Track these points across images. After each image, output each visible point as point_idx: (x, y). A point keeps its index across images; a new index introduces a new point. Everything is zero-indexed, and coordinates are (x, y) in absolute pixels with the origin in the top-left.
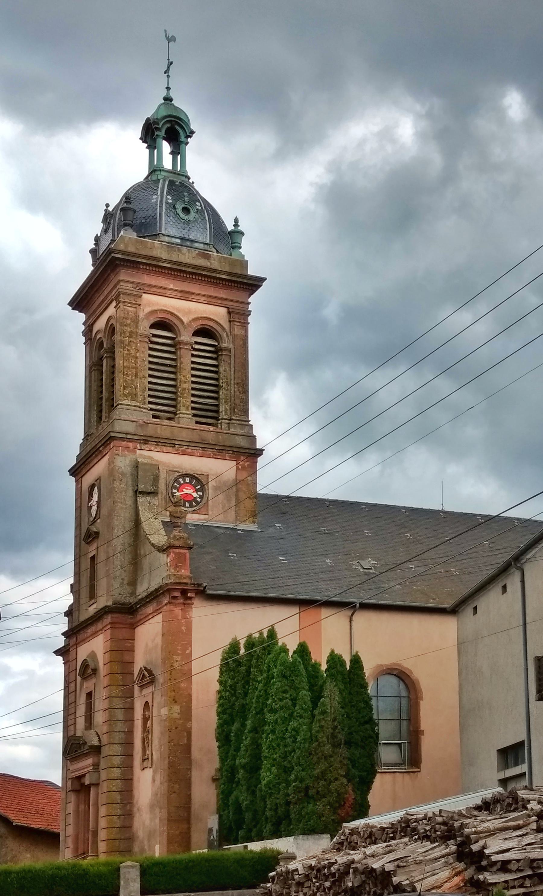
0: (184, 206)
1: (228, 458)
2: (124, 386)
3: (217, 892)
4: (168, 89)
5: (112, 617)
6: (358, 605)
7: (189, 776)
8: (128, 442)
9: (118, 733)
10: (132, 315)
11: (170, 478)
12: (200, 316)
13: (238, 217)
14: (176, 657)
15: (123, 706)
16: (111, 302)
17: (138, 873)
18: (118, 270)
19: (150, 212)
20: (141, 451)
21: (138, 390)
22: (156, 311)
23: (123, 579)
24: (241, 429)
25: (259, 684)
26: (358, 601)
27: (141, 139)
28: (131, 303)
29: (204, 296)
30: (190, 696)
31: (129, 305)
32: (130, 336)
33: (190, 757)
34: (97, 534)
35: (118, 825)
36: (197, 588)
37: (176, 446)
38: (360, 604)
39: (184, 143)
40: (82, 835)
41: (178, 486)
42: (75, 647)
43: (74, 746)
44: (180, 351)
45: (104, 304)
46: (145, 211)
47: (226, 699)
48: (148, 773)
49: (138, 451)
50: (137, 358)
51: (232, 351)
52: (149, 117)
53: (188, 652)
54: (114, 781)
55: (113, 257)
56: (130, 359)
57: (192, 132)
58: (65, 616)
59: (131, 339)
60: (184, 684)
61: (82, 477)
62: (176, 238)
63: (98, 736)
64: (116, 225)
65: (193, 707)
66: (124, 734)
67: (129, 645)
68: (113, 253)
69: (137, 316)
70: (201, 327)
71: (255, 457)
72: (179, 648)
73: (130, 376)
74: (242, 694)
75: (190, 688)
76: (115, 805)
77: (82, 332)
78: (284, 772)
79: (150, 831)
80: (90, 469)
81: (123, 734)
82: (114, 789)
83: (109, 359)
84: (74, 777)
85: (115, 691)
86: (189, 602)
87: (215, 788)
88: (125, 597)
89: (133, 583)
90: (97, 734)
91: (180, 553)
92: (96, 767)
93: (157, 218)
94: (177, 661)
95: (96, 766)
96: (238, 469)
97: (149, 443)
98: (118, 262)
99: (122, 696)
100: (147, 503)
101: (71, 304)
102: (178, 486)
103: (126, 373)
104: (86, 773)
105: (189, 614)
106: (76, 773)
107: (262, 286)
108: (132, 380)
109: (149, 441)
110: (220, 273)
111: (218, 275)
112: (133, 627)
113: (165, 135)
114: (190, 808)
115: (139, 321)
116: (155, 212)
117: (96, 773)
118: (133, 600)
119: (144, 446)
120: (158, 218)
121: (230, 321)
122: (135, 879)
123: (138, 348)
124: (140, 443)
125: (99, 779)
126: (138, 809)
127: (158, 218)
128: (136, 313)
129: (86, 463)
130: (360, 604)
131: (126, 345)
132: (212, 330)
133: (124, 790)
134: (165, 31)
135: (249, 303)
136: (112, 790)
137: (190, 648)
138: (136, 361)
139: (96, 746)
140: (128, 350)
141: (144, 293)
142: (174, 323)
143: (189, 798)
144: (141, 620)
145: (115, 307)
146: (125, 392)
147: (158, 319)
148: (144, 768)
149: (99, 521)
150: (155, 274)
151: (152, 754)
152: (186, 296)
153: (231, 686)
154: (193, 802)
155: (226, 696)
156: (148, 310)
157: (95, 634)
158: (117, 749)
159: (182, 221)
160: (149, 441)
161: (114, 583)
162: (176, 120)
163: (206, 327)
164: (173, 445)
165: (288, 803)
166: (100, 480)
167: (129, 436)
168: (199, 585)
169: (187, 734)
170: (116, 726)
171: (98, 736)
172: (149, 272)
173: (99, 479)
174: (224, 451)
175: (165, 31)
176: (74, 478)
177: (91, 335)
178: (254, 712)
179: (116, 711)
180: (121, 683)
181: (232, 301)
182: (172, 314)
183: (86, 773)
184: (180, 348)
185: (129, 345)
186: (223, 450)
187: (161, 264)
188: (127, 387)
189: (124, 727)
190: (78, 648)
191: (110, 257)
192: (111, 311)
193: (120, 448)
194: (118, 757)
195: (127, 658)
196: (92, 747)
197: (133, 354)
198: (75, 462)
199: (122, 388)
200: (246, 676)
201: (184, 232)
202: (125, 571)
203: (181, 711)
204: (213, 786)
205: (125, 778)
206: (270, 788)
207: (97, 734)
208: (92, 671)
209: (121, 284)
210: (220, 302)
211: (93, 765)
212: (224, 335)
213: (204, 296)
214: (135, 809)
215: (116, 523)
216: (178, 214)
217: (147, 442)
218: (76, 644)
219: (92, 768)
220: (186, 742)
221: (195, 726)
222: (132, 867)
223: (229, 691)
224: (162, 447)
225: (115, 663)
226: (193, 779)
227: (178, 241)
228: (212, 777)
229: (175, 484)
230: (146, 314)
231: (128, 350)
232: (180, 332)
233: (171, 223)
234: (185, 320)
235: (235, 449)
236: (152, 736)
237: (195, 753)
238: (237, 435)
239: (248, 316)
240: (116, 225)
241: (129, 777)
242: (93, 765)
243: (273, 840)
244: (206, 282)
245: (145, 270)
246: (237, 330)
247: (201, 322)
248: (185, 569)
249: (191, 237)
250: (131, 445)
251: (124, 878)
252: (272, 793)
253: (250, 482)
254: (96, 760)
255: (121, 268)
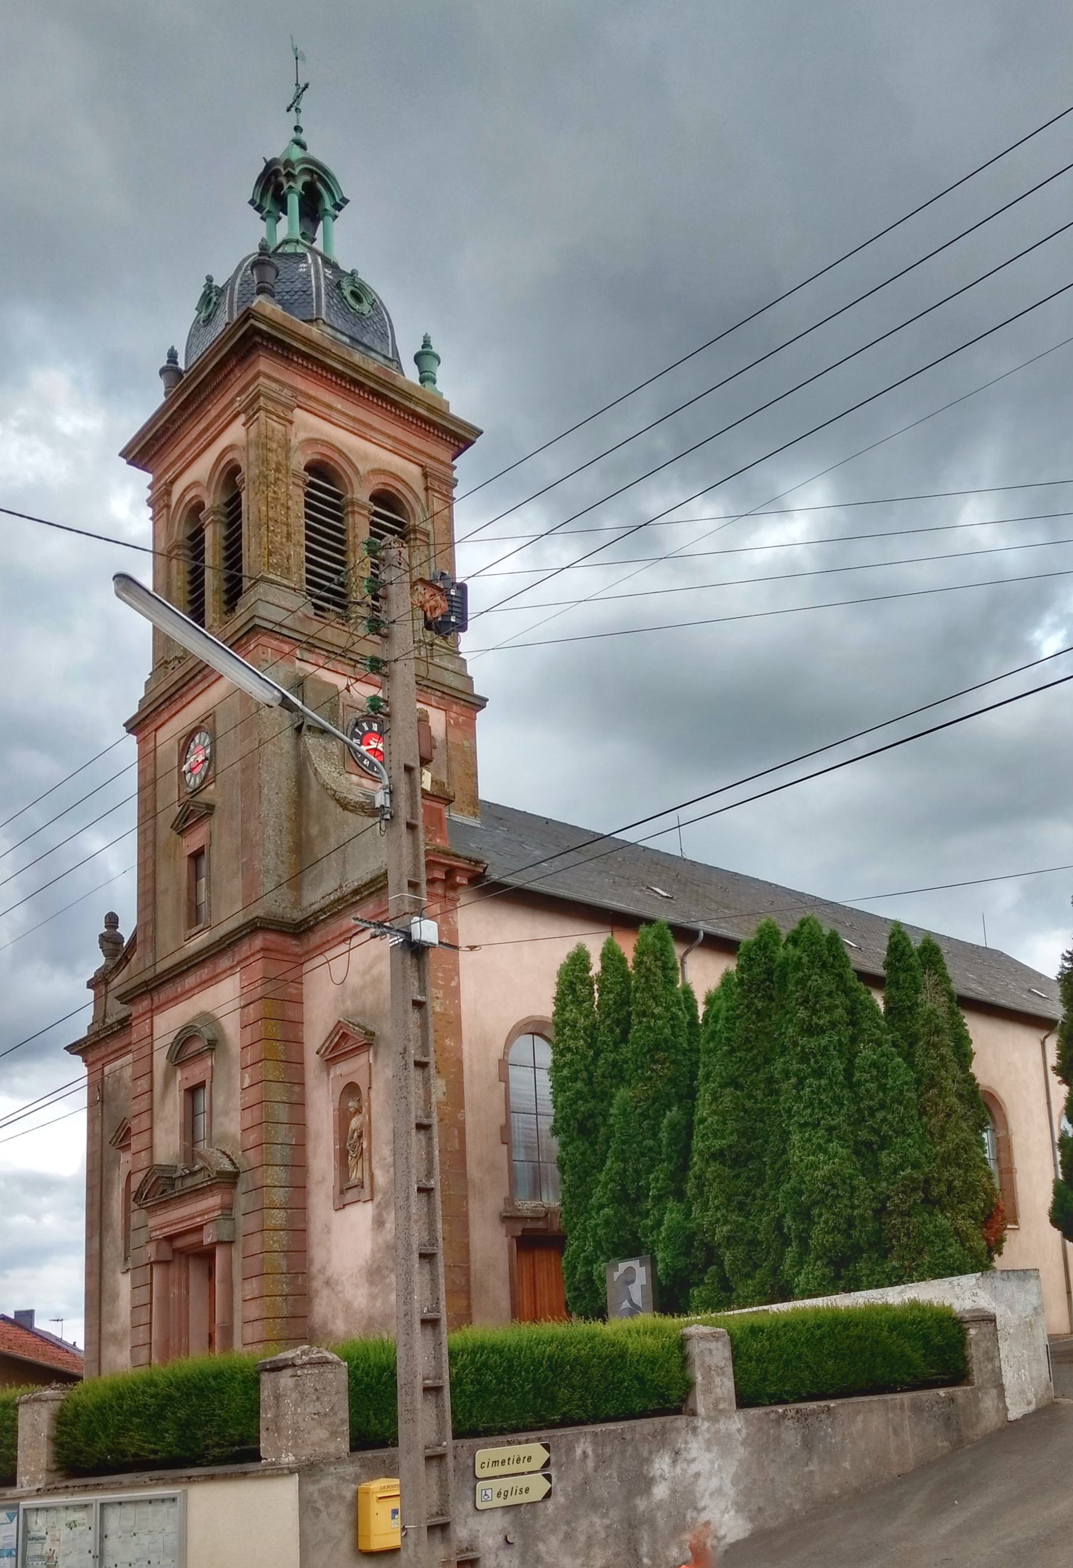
0: (353, 288)
1: (434, 704)
2: (269, 551)
3: (875, 1398)
4: (297, 129)
5: (265, 939)
6: (702, 934)
7: (464, 1209)
8: (282, 641)
9: (279, 1146)
10: (279, 436)
11: (349, 718)
12: (382, 467)
13: (429, 335)
14: (437, 991)
15: (288, 1098)
16: (236, 416)
17: (728, 1353)
18: (253, 357)
19: (299, 285)
20: (303, 663)
21: (292, 561)
22: (317, 440)
23: (279, 876)
24: (449, 663)
25: (655, 1021)
26: (703, 927)
27: (252, 202)
28: (278, 416)
29: (389, 436)
30: (460, 1062)
31: (275, 418)
32: (277, 470)
33: (464, 1175)
34: (210, 808)
35: (285, 1313)
36: (472, 868)
37: (359, 666)
38: (706, 934)
39: (330, 215)
40: (176, 1340)
41: (361, 733)
42: (149, 1015)
43: (160, 1182)
44: (353, 518)
45: (208, 434)
46: (288, 283)
47: (577, 1053)
48: (361, 1215)
49: (297, 662)
50: (288, 508)
51: (432, 535)
52: (277, 156)
53: (453, 984)
54: (276, 1232)
55: (251, 325)
56: (278, 507)
57: (345, 201)
58: (89, 987)
59: (278, 475)
60: (450, 1041)
61: (156, 730)
62: (343, 333)
63: (228, 1156)
64: (235, 300)
65: (466, 1085)
66: (291, 1149)
67: (294, 992)
68: (253, 318)
69: (288, 441)
70: (383, 487)
71: (473, 709)
72: (440, 975)
73: (279, 537)
74: (611, 1043)
75: (459, 1049)
76: (278, 1277)
77: (148, 500)
78: (854, 1153)
79: (370, 1318)
80: (163, 724)
81: (287, 1149)
82: (276, 1247)
83: (218, 525)
84: (161, 1237)
85: (272, 1071)
86: (451, 894)
87: (504, 1233)
88: (284, 908)
89: (296, 881)
90: (224, 1153)
91: (432, 808)
92: (227, 1212)
93: (312, 294)
94: (437, 998)
95: (227, 1209)
96: (447, 723)
97: (317, 650)
98: (258, 339)
99: (284, 1080)
100: (320, 748)
101: (124, 454)
102: (361, 733)
103: (272, 528)
104: (206, 1224)
105: (452, 917)
106: (166, 1230)
107: (473, 442)
108: (282, 543)
109: (317, 647)
110: (417, 404)
111: (412, 406)
112: (300, 961)
113: (303, 189)
114: (469, 1268)
115: (290, 448)
116: (309, 285)
117: (228, 1222)
118: (298, 916)
119: (307, 656)
120: (314, 295)
121: (427, 489)
122: (722, 1368)
123: (290, 492)
124: (302, 648)
125: (234, 1232)
126: (327, 1283)
127: (314, 295)
128: (285, 435)
129: (173, 699)
130: (706, 934)
131: (271, 483)
132: (400, 497)
133: (291, 1249)
134: (292, 37)
135: (454, 468)
136: (272, 1249)
137: (456, 978)
138: (287, 513)
139: (230, 1172)
140: (275, 492)
141: (298, 406)
142: (343, 469)
143: (466, 1248)
144: (328, 941)
145: (244, 425)
146: (271, 561)
147: (318, 457)
148: (344, 1205)
149: (212, 787)
150: (315, 378)
151: (372, 1176)
152: (361, 429)
153: (585, 1029)
154: (472, 1259)
155: (577, 1048)
156: (303, 435)
157: (214, 979)
158: (277, 1175)
159: (352, 310)
160: (317, 647)
161: (265, 880)
162: (322, 174)
163: (390, 489)
164: (353, 663)
165: (880, 1212)
166: (215, 716)
167: (285, 631)
168: (478, 862)
169: (459, 1133)
170: (276, 1133)
171: (228, 1156)
172: (307, 373)
173: (210, 715)
174: (429, 691)
175: (292, 37)
176: (135, 737)
177: (169, 500)
178: (725, 1048)
179: (276, 1106)
180: (283, 1058)
181: (430, 457)
182: (340, 452)
183: (206, 1224)
184: (353, 512)
185: (275, 484)
186: (428, 687)
187: (329, 361)
188: (275, 553)
189: (291, 1135)
190: (154, 1018)
191: (246, 327)
192: (236, 433)
193: (270, 650)
194: (282, 1189)
195: (291, 1014)
196: (221, 1174)
197: (282, 501)
198: (137, 710)
199: (266, 552)
200: (615, 1011)
201: (355, 329)
202: (282, 862)
203: (447, 1088)
204: (502, 1230)
205: (294, 1228)
206: (834, 1186)
207: (224, 1153)
208: (209, 1044)
209: (262, 379)
210: (411, 453)
211: (221, 1208)
212: (418, 509)
213: (389, 436)
214: (317, 1284)
215: (266, 776)
216: (345, 298)
217: (313, 649)
218: (152, 1010)
219: (219, 1212)
220: (457, 1146)
221: (470, 1119)
222: (715, 1337)
223: (582, 1037)
224: (336, 663)
225: (273, 1022)
226: (471, 1215)
227: (347, 340)
228: (500, 1215)
229: (357, 730)
230: (303, 441)
231: (275, 492)
232: (352, 485)
233: (335, 308)
234: (362, 468)
235: (446, 690)
236: (370, 1144)
237: (473, 1170)
238: (446, 670)
239: (454, 487)
240: (235, 300)
241: (301, 1226)
242: (221, 1208)
243: (880, 1290)
244: (393, 416)
245: (300, 368)
246: (437, 505)
247: (383, 479)
248: (441, 838)
249: (365, 341)
250: (286, 648)
251: (702, 1365)
252: (838, 1196)
253: (466, 749)
254: (227, 1199)
255: (261, 353)
